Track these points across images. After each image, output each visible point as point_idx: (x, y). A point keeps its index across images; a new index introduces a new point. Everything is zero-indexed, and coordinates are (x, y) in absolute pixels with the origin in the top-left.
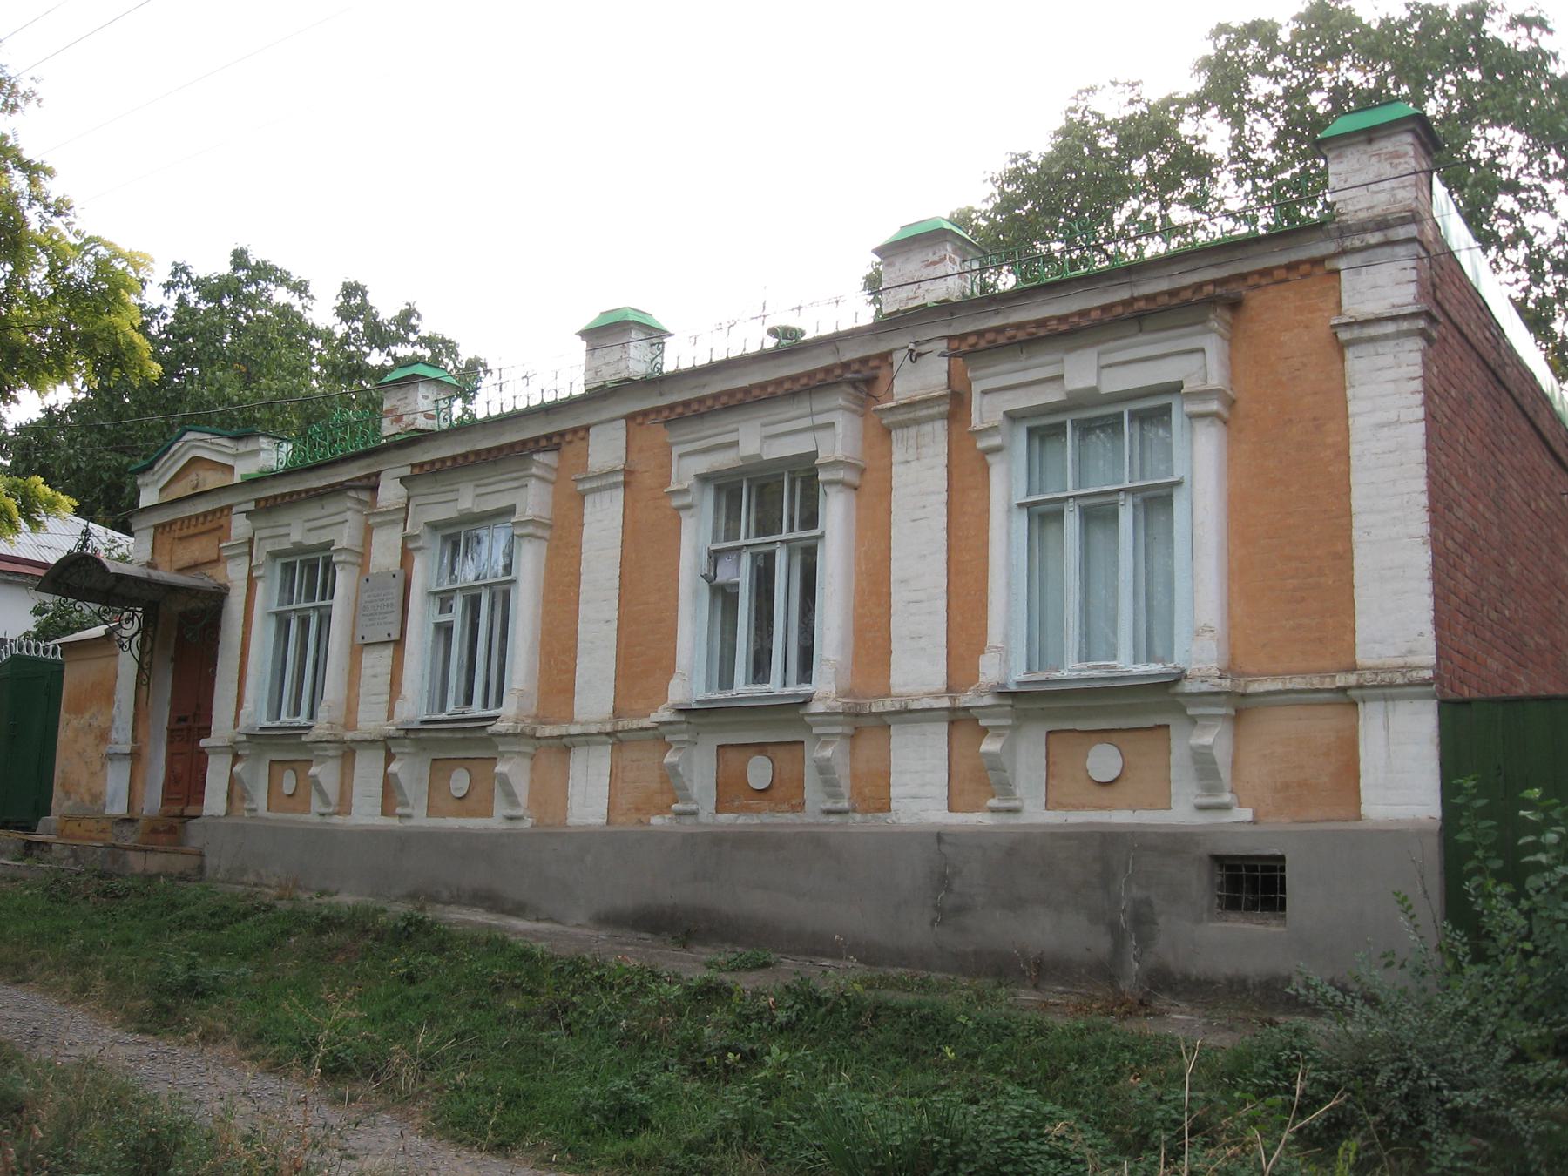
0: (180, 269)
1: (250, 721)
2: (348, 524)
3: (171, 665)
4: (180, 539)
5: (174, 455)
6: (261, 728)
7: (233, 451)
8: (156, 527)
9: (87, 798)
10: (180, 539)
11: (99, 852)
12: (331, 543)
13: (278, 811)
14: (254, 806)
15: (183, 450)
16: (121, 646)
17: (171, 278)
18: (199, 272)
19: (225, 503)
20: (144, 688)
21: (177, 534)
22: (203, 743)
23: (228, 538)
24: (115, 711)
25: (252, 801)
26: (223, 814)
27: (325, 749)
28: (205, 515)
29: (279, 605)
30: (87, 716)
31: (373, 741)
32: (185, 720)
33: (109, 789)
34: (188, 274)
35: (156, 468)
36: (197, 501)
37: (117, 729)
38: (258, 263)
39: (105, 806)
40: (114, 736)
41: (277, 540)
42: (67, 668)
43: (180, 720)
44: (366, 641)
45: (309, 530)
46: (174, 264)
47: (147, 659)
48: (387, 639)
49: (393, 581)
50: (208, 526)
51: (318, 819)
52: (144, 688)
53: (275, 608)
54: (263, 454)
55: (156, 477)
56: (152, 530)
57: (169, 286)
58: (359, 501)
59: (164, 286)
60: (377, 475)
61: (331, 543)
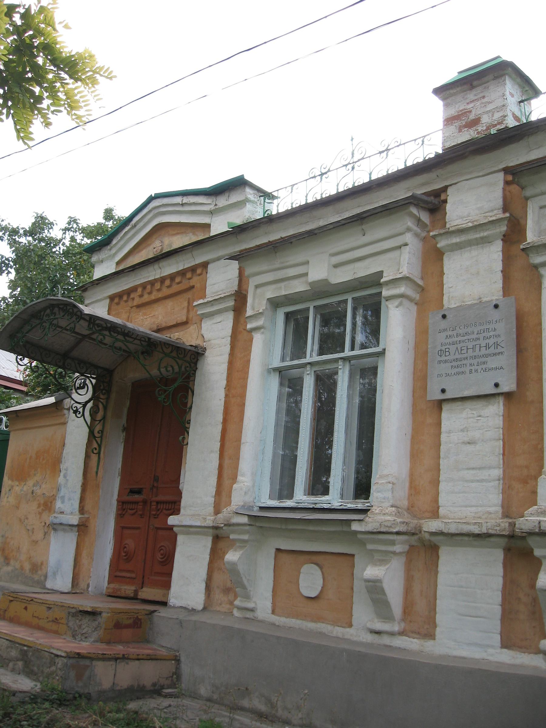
0: (73, 220)
1: (248, 499)
2: (406, 250)
3: (123, 435)
4: (139, 306)
5: (135, 226)
6: (261, 508)
7: (212, 207)
8: (112, 298)
9: (27, 566)
10: (139, 306)
11: (60, 662)
12: (380, 274)
13: (288, 616)
14: (250, 605)
15: (146, 220)
16: (75, 412)
17: (67, 225)
18: (83, 223)
19: (199, 260)
20: (94, 458)
21: (137, 301)
22: (172, 520)
23: (204, 297)
24: (61, 479)
25: (247, 597)
26: (200, 607)
27: (393, 543)
28: (172, 277)
29: (283, 359)
30: (30, 483)
31: (488, 535)
32: (139, 492)
33: (52, 559)
34: (77, 223)
35: (114, 242)
36: (163, 263)
37: (63, 498)
38: (118, 217)
39: (46, 577)
40: (59, 505)
41: (282, 285)
42: (11, 438)
43: (133, 492)
44: (448, 395)
45: (336, 266)
46: (70, 217)
47: (98, 428)
48: (494, 391)
49: (496, 315)
50: (175, 288)
51: (369, 638)
52: (94, 458)
53: (277, 363)
54: (249, 206)
55: (113, 251)
56: (108, 301)
57: (66, 230)
58: (419, 221)
59: (63, 230)
60: (445, 189)
61: (380, 274)
